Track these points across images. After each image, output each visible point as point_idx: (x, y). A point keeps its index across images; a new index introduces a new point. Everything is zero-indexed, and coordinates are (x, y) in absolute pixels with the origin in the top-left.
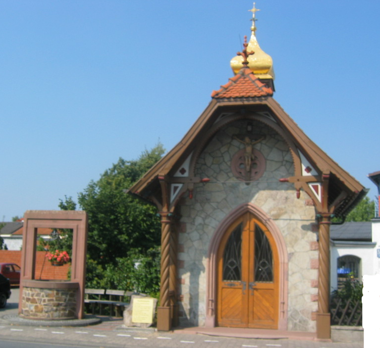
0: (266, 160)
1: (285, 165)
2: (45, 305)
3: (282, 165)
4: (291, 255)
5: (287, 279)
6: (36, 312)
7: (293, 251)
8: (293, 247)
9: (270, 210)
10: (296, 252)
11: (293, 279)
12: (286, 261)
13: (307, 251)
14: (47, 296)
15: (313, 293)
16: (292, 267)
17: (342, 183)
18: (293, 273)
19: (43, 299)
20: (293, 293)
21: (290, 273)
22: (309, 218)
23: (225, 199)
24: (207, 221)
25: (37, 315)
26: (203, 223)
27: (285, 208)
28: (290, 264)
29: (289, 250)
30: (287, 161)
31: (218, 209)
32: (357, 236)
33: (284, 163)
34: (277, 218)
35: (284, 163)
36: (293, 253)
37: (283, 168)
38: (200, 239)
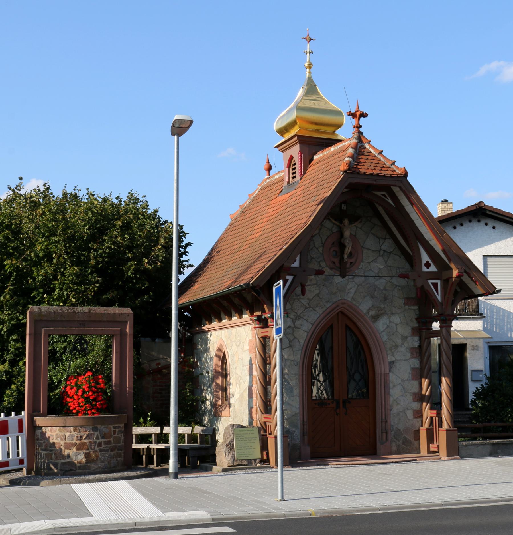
0: (362, 247)
1: (382, 255)
2: (101, 450)
3: (380, 256)
4: (392, 363)
5: (389, 393)
6: (87, 462)
7: (394, 359)
8: (393, 355)
9: (369, 310)
10: (396, 360)
11: (395, 392)
12: (387, 371)
13: (407, 360)
14: (103, 437)
15: (415, 409)
16: (392, 377)
17: (413, 188)
18: (394, 386)
19: (98, 441)
20: (395, 410)
21: (391, 385)
22: (351, 136)
23: (318, 295)
24: (298, 323)
25: (89, 468)
26: (293, 326)
27: (384, 308)
28: (391, 374)
29: (390, 358)
30: (384, 251)
31: (310, 307)
32: (504, 485)
33: (382, 252)
34: (376, 318)
35: (382, 252)
36: (393, 362)
37: (381, 258)
38: (290, 346)
